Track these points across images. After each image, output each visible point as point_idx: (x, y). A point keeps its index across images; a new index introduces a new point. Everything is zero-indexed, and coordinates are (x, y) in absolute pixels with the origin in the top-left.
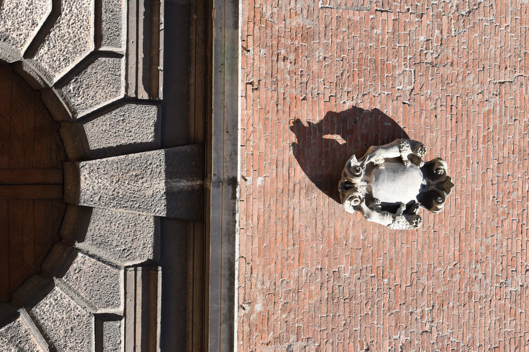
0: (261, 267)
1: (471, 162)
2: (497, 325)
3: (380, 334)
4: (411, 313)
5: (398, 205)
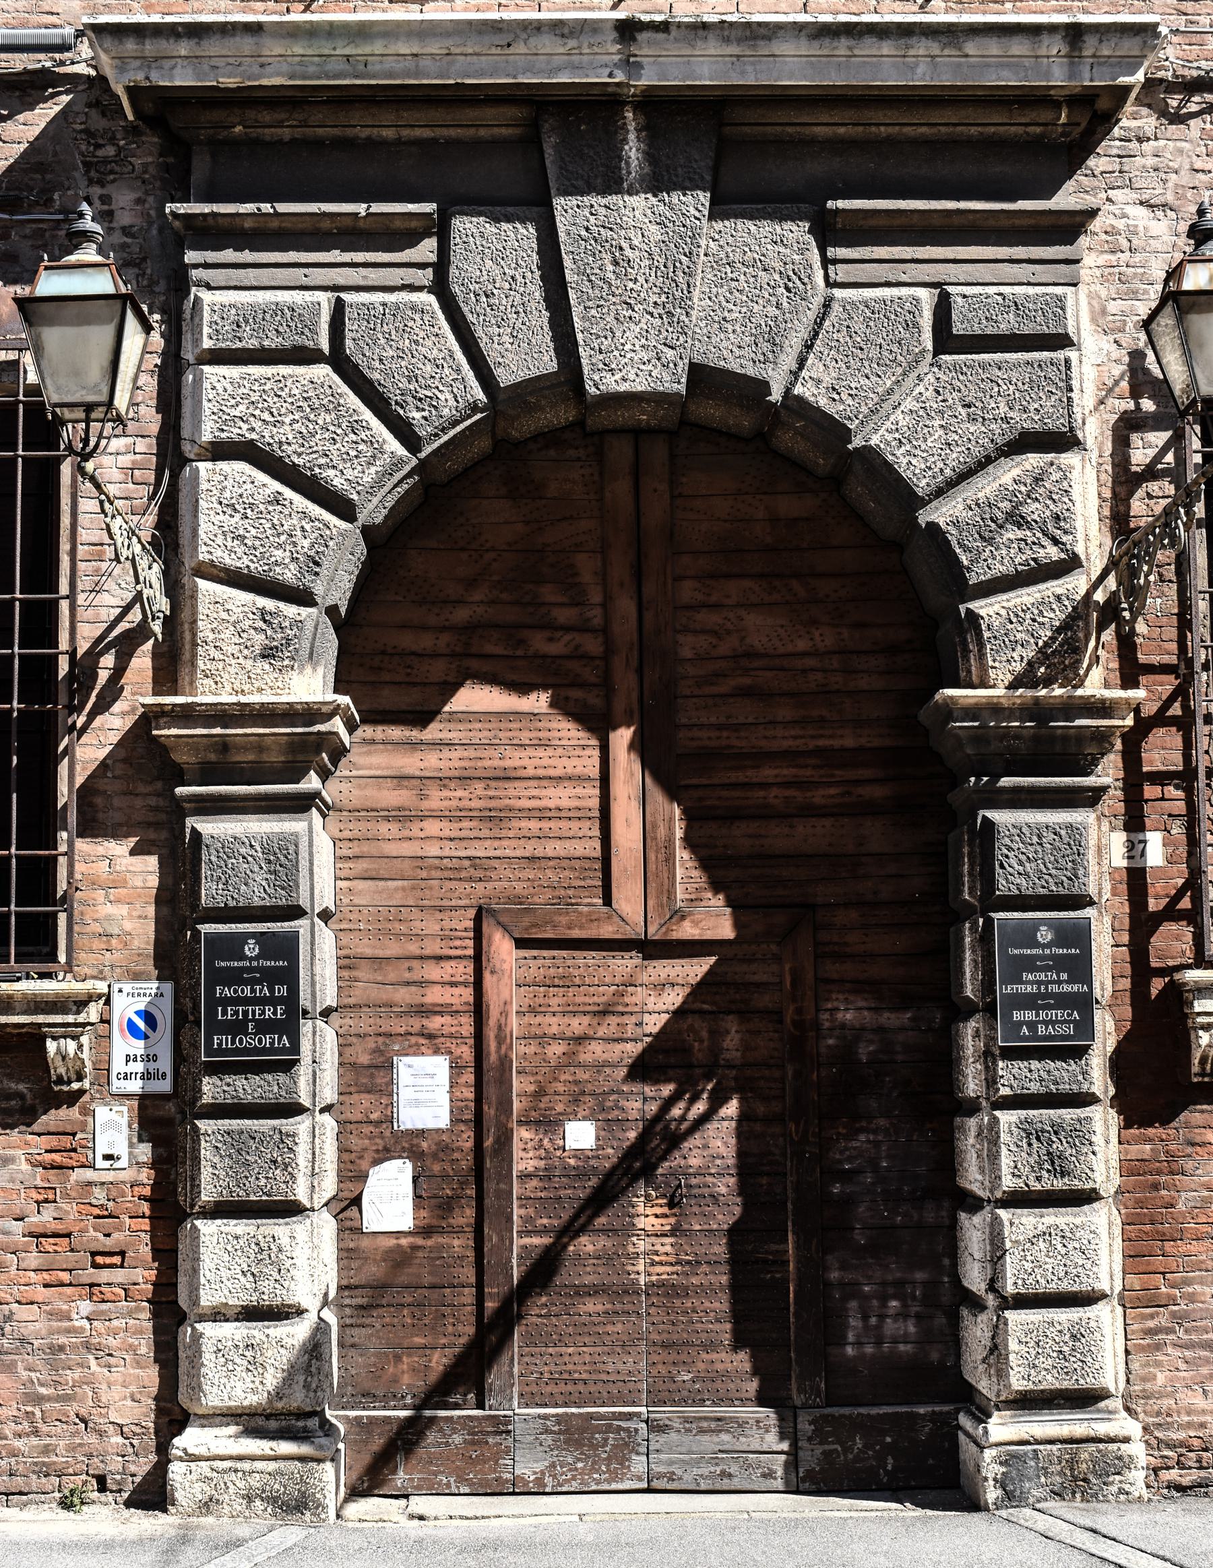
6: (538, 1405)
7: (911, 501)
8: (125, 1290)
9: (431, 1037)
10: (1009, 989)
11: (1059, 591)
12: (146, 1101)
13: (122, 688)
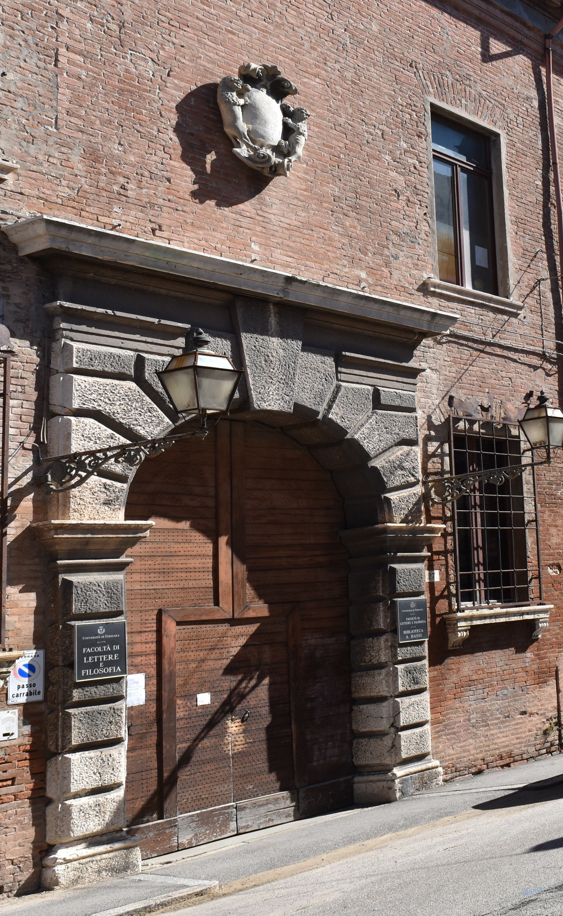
0: (332, 265)
1: (230, 28)
2: (378, 68)
3: (385, 177)
4: (368, 142)
5: (285, 125)
6: (186, 812)
7: (367, 457)
8: (14, 795)
9: (136, 666)
10: (402, 624)
11: (415, 492)
12: (26, 706)
13: (15, 516)
